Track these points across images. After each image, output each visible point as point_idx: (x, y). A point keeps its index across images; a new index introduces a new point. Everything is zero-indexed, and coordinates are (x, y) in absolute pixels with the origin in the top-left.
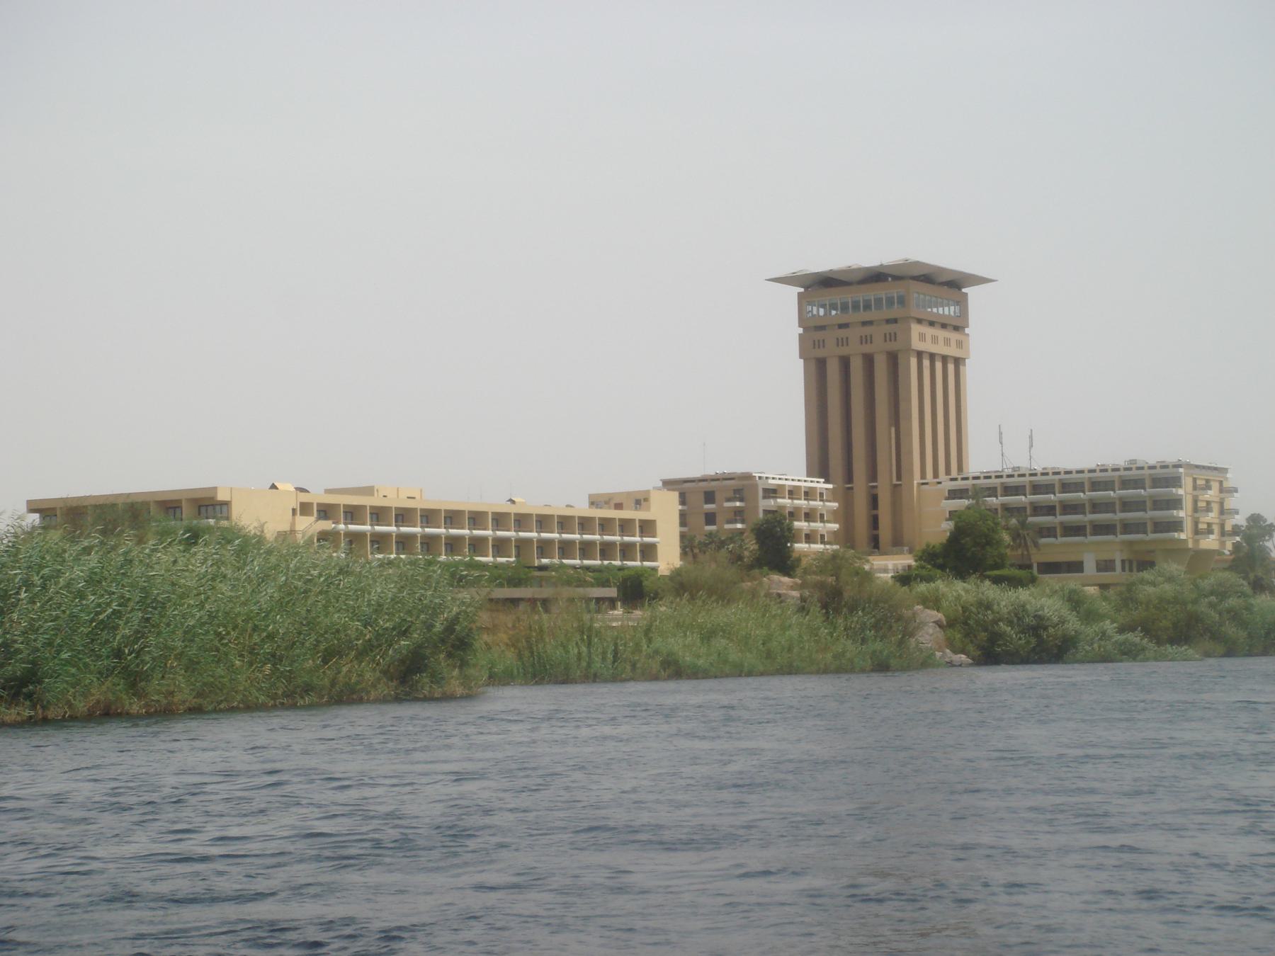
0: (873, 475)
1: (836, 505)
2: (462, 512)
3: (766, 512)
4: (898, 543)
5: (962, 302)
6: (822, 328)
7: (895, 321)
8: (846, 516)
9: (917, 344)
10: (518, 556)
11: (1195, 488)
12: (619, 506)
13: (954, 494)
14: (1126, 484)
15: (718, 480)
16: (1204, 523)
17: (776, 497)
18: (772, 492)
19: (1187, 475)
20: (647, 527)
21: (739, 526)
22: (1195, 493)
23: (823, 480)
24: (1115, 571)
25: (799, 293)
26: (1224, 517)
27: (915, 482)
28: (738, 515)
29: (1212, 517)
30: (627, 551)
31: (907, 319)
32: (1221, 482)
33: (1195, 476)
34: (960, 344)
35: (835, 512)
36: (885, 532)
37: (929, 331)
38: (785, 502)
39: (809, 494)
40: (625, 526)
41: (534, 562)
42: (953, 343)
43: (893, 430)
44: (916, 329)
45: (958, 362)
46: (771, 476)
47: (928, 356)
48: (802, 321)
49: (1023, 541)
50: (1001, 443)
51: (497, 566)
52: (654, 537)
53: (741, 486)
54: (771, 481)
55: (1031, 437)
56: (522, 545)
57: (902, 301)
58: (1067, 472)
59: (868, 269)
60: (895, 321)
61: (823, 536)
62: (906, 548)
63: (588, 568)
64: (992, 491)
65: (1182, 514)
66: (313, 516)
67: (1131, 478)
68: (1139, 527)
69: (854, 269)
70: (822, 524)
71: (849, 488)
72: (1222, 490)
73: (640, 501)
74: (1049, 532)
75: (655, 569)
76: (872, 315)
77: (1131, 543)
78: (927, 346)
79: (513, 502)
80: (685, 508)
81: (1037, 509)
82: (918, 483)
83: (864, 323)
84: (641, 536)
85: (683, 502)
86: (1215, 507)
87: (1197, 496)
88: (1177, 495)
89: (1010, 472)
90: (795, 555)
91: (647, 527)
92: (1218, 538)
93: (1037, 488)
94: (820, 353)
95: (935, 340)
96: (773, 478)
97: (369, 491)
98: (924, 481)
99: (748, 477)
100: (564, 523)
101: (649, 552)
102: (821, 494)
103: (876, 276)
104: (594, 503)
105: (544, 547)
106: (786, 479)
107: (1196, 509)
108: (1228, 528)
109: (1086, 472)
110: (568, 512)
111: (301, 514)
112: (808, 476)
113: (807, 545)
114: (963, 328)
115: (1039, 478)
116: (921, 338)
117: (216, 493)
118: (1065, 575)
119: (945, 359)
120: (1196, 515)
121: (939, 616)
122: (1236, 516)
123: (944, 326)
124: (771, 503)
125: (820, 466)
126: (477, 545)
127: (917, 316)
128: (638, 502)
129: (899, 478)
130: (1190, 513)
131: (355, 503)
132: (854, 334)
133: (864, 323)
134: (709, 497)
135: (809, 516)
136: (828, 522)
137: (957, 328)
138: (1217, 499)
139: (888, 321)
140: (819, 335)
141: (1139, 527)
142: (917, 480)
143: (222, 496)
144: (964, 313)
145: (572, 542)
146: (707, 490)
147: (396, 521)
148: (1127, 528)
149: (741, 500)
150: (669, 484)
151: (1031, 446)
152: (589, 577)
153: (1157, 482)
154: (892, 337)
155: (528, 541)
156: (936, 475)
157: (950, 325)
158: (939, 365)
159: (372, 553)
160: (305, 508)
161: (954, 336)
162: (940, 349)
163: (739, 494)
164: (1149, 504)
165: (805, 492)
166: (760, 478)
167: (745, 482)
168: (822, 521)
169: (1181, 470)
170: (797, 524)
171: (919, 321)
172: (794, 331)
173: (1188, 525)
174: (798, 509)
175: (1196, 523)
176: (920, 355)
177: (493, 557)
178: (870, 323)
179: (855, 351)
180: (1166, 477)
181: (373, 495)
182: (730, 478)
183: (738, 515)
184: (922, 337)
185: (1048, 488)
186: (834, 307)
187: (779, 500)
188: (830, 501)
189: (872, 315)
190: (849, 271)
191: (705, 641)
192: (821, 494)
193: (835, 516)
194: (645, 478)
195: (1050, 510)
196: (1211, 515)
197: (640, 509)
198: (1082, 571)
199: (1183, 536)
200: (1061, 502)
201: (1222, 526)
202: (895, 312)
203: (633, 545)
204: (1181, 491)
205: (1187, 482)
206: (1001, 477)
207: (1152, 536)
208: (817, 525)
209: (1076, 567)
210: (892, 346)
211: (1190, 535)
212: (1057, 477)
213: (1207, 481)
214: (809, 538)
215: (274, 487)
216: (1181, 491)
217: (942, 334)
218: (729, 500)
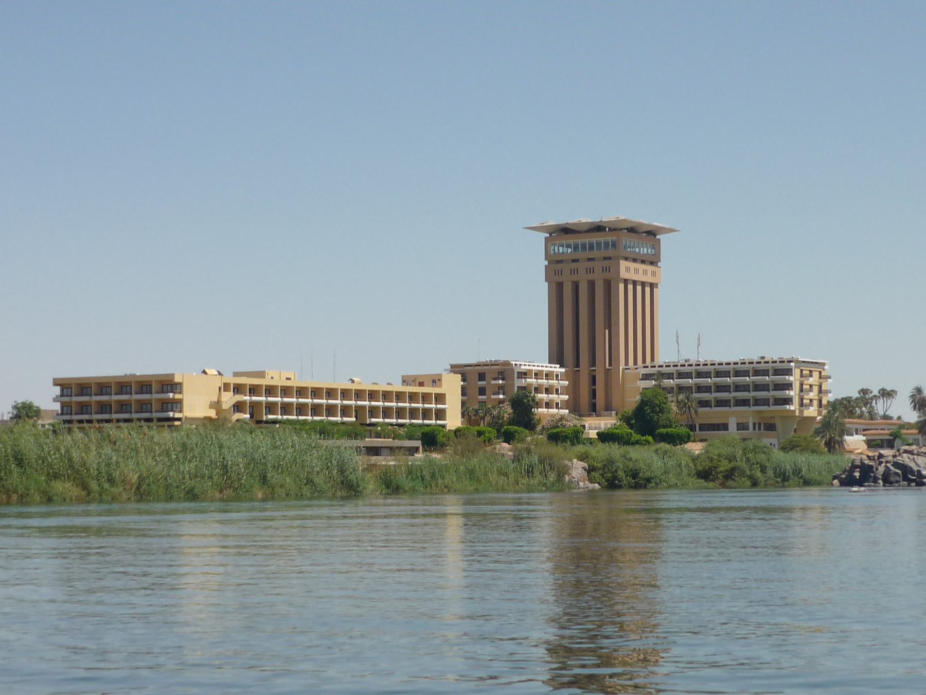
0: (593, 363)
1: (567, 382)
2: (307, 388)
3: (520, 388)
4: (608, 408)
5: (656, 245)
6: (561, 262)
7: (610, 258)
8: (573, 390)
9: (624, 274)
10: (356, 417)
11: (802, 376)
12: (421, 384)
13: (646, 377)
15: (480, 365)
16: (807, 399)
17: (526, 378)
18: (523, 375)
19: (796, 367)
20: (440, 398)
21: (501, 396)
22: (802, 379)
23: (559, 366)
24: (748, 430)
25: (546, 238)
26: (821, 395)
27: (621, 368)
28: (501, 389)
29: (813, 395)
30: (426, 414)
31: (618, 258)
32: (820, 372)
33: (802, 368)
34: (654, 274)
35: (567, 388)
36: (600, 401)
38: (532, 381)
39: (548, 376)
40: (426, 398)
41: (263, 418)
42: (649, 273)
43: (607, 331)
44: (623, 264)
45: (652, 286)
46: (523, 363)
47: (632, 282)
48: (547, 256)
49: (687, 410)
50: (678, 343)
51: (313, 422)
52: (444, 404)
53: (504, 371)
54: (522, 367)
55: (699, 339)
56: (359, 410)
57: (614, 245)
59: (592, 223)
60: (610, 258)
61: (557, 404)
62: (614, 412)
63: (401, 425)
64: (670, 376)
65: (792, 393)
66: (230, 391)
68: (765, 402)
69: (583, 223)
70: (557, 396)
71: (577, 371)
72: (820, 377)
73: (436, 381)
74: (704, 404)
75: (444, 426)
76: (595, 254)
77: (760, 412)
78: (632, 276)
79: (353, 381)
80: (466, 383)
81: (700, 389)
82: (623, 369)
83: (589, 260)
84: (436, 404)
85: (463, 380)
86: (816, 389)
87: (803, 381)
88: (790, 381)
89: (682, 362)
90: (537, 417)
91: (440, 398)
92: (817, 409)
93: (699, 375)
95: (637, 271)
96: (525, 365)
97: (261, 375)
98: (627, 367)
99: (507, 364)
100: (386, 396)
101: (440, 414)
102: (557, 376)
103: (598, 228)
104: (405, 382)
105: (373, 411)
106: (533, 366)
107: (801, 390)
108: (824, 402)
109: (732, 364)
110: (375, 388)
111: (224, 391)
112: (549, 363)
113: (546, 410)
114: (657, 263)
115: (701, 367)
116: (628, 270)
117: (174, 378)
118: (716, 432)
119: (643, 284)
120: (802, 394)
121: (586, 465)
122: (829, 395)
123: (643, 262)
124: (523, 382)
125: (557, 357)
126: (331, 410)
127: (625, 256)
128: (434, 381)
129: (610, 365)
130: (797, 393)
131: (256, 383)
132: (582, 266)
133: (589, 260)
134: (482, 377)
135: (548, 391)
136: (561, 394)
137: (652, 263)
138: (818, 383)
139: (605, 259)
141: (765, 402)
143: (177, 379)
145: (306, 405)
147: (250, 393)
148: (757, 402)
149: (503, 379)
150: (455, 369)
151: (699, 345)
152: (402, 431)
153: (777, 372)
154: (606, 269)
155: (363, 407)
156: (635, 363)
157: (648, 261)
158: (639, 288)
159: (266, 414)
160: (226, 387)
161: (650, 268)
162: (640, 277)
163: (502, 375)
164: (771, 387)
165: (546, 374)
166: (515, 365)
167: (506, 367)
168: (557, 393)
169: (792, 364)
170: (540, 396)
171: (626, 259)
172: (542, 263)
173: (796, 400)
174: (541, 385)
175: (802, 399)
176: (626, 282)
177: (435, 420)
179: (583, 280)
181: (265, 377)
182: (495, 364)
183: (501, 389)
184: (628, 270)
185: (707, 375)
186: (568, 246)
187: (528, 380)
188: (563, 380)
189: (595, 254)
190: (580, 224)
191: (358, 494)
192: (557, 376)
193: (566, 390)
194: (437, 364)
195: (707, 389)
196: (811, 394)
197: (435, 386)
198: (727, 429)
199: (792, 408)
200: (715, 384)
201: (820, 401)
202: (610, 252)
203: (430, 410)
204: (792, 378)
205: (797, 372)
206: (677, 366)
207: (773, 408)
208: (554, 396)
209: (725, 427)
210: (607, 275)
211: (797, 407)
212: (713, 367)
213: (811, 371)
214: (548, 405)
215: (204, 372)
216: (792, 378)
217: (641, 267)
218: (495, 379)
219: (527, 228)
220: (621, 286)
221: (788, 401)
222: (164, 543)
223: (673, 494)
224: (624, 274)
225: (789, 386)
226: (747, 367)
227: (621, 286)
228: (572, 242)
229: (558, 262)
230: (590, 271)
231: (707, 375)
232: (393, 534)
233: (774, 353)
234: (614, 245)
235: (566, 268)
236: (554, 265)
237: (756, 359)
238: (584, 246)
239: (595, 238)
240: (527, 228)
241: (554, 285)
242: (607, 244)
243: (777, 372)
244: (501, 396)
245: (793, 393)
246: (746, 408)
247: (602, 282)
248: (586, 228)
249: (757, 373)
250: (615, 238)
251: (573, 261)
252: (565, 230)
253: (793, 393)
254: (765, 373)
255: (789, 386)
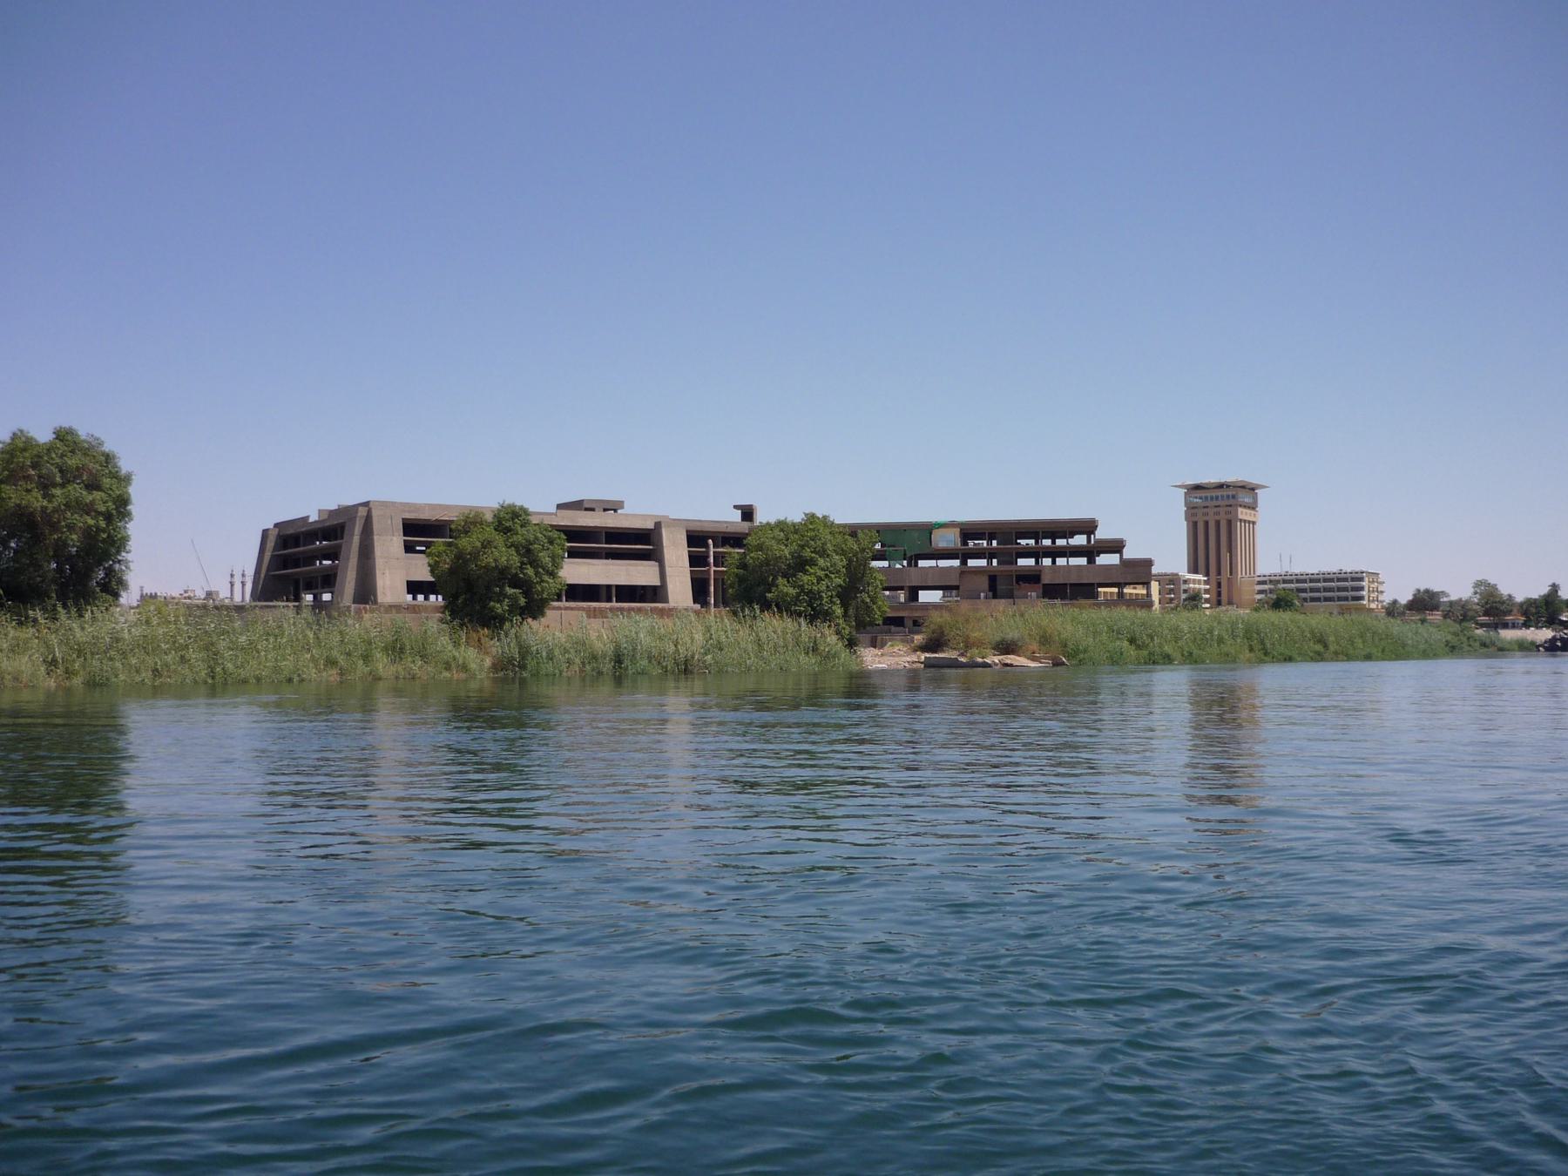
0: (1219, 573)
7: (1230, 506)
9: (1240, 517)
11: (1369, 582)
14: (1339, 580)
21: (1173, 596)
37: (1245, 510)
45: (1254, 523)
50: (1281, 560)
57: (1234, 497)
58: (1312, 574)
60: (1230, 506)
67: (1341, 577)
68: (1346, 599)
77: (1340, 605)
83: (1216, 507)
89: (1283, 573)
93: (1298, 581)
94: (1195, 519)
103: (1221, 486)
116: (1243, 514)
119: (1249, 522)
125: (1194, 569)
129: (1231, 574)
137: (1254, 509)
140: (1193, 511)
141: (1346, 599)
142: (1239, 576)
144: (1255, 502)
146: (693, 527)
148: (1340, 599)
153: (1353, 579)
156: (1246, 574)
161: (1253, 512)
171: (1240, 506)
176: (1241, 520)
178: (1219, 506)
180: (1357, 577)
185: (1304, 581)
190: (1210, 483)
199: (1365, 603)
202: (1231, 501)
210: (1229, 517)
219: (1176, 486)
220: (1239, 523)
221: (1362, 598)
222: (870, 702)
223: (236, 870)
224: (1240, 517)
225: (1362, 588)
226: (1331, 576)
227: (1239, 523)
228: (1203, 495)
229: (1193, 508)
230: (1218, 513)
231: (1304, 581)
232: (351, 818)
233: (1349, 566)
234: (1234, 497)
235: (1200, 512)
236: (1191, 510)
237: (1316, 571)
238: (1212, 498)
239: (1219, 493)
240: (1176, 486)
241: (1191, 523)
242: (1228, 496)
243: (1353, 579)
244: (1173, 596)
245: (1364, 593)
246: (1332, 603)
247: (1225, 521)
248: (1214, 485)
249: (1339, 580)
250: (1234, 493)
251: (1204, 507)
252: (1198, 487)
253: (1364, 593)
254: (1345, 580)
255: (1362, 588)
